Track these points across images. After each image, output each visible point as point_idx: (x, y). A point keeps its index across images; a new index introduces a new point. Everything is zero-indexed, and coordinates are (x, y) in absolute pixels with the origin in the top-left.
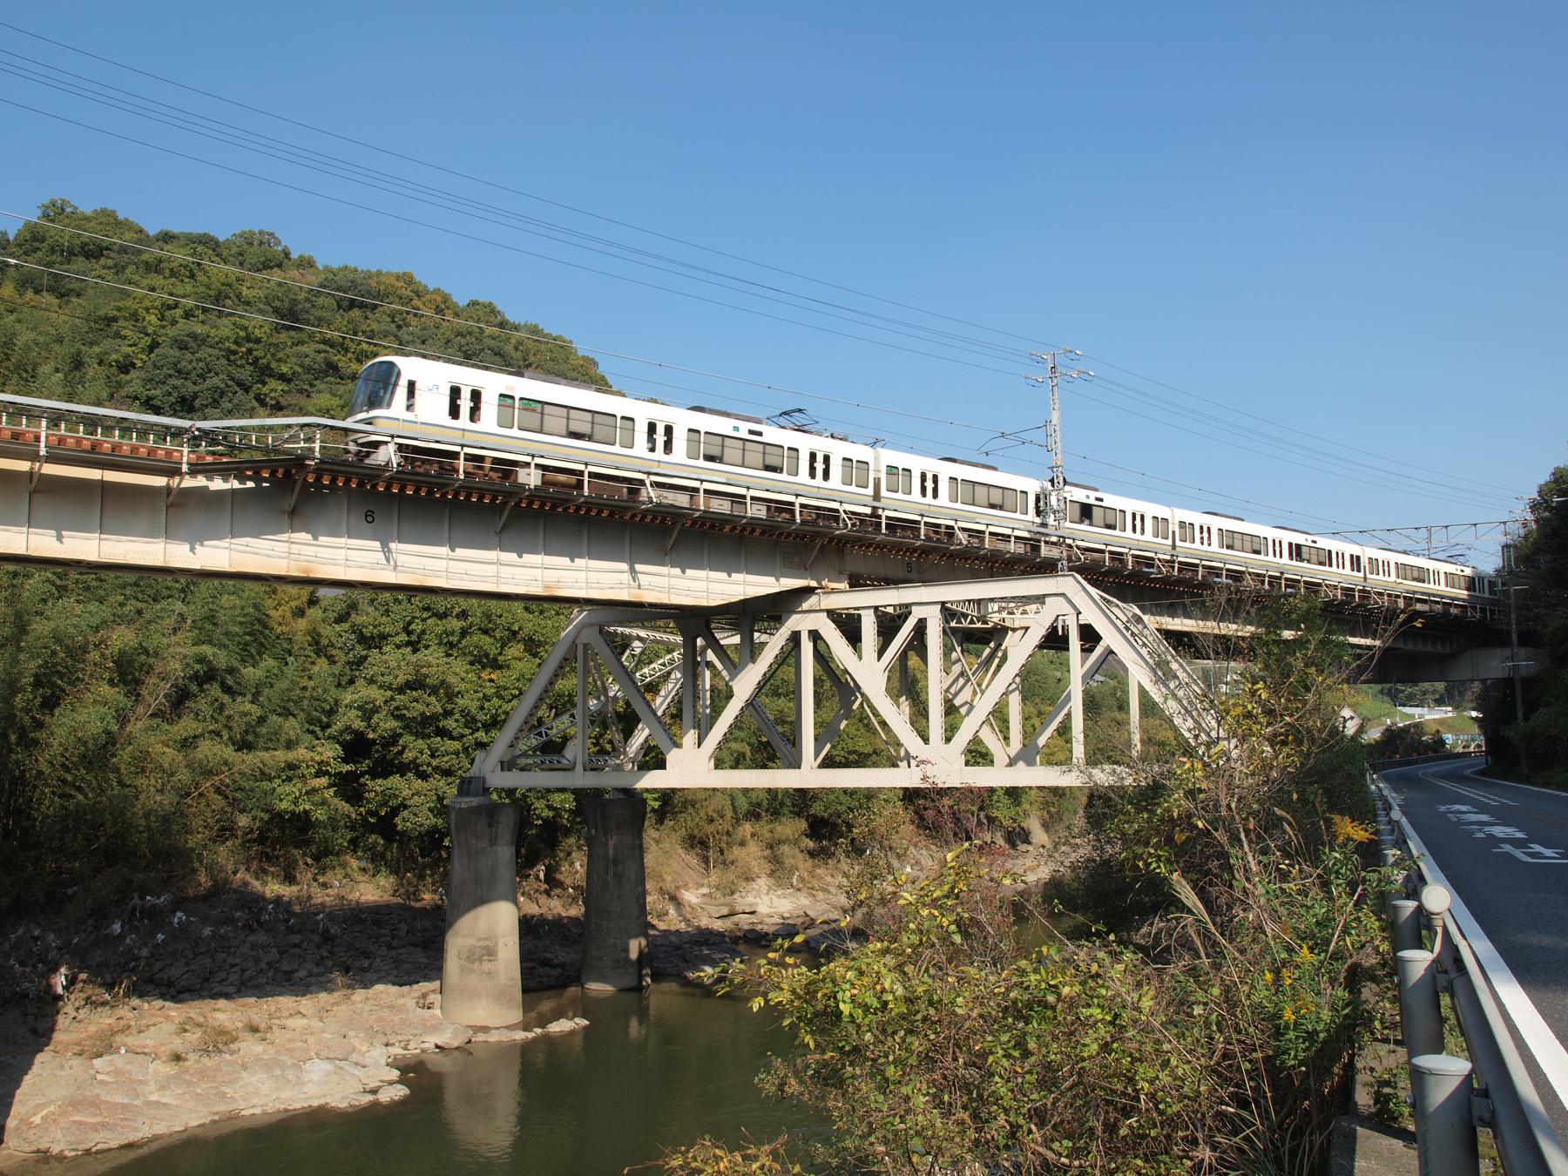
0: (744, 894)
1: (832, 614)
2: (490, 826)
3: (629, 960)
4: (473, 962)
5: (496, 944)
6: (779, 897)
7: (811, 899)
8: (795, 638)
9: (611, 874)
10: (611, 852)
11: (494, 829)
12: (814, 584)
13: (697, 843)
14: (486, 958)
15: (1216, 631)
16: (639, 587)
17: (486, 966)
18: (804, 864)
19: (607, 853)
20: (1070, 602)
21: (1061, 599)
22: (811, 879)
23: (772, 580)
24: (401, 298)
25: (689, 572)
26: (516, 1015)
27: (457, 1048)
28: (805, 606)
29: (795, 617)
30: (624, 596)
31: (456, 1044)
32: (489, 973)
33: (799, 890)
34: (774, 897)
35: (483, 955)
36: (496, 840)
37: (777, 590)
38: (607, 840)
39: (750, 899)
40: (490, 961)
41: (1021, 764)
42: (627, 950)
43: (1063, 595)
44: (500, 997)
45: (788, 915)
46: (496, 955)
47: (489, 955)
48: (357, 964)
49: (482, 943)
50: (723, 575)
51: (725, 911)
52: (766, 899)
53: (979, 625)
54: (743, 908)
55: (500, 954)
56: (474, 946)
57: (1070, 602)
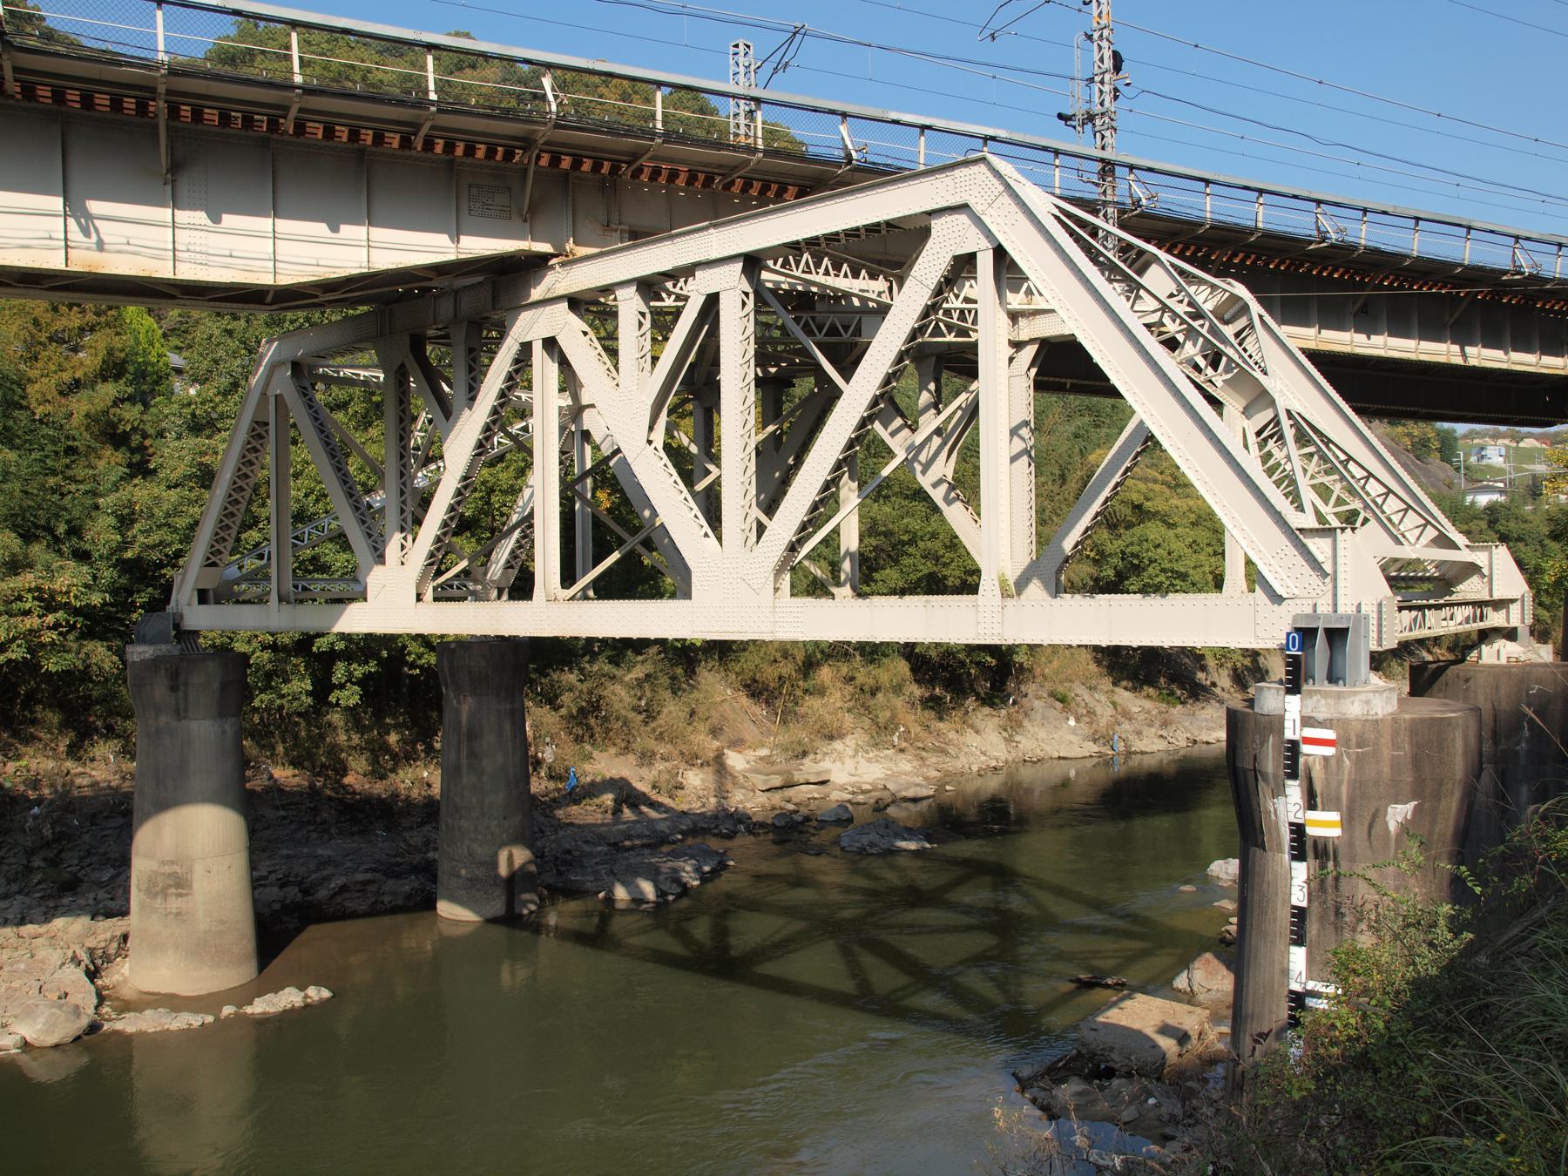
0: (819, 757)
1: (576, 303)
2: (174, 688)
3: (497, 876)
4: (155, 896)
5: (191, 871)
6: (869, 760)
7: (916, 763)
8: (524, 356)
9: (464, 753)
10: (464, 718)
11: (181, 694)
12: (545, 248)
13: (756, 690)
14: (173, 890)
15: (1459, 361)
16: (100, 245)
17: (174, 904)
18: (911, 720)
19: (459, 722)
20: (978, 221)
21: (962, 219)
22: (923, 735)
23: (442, 240)
24: (587, 86)
25: (229, 220)
26: (237, 972)
27: (56, 1046)
28: (536, 294)
29: (525, 316)
30: (54, 261)
31: (51, 1040)
32: (178, 914)
33: (902, 751)
34: (863, 761)
35: (169, 886)
36: (186, 709)
37: (452, 257)
38: (459, 703)
39: (826, 764)
40: (180, 895)
41: (1035, 589)
42: (495, 865)
43: (963, 208)
44: (201, 950)
45: (869, 787)
46: (190, 887)
47: (178, 885)
48: (95, 876)
49: (167, 869)
50: (320, 229)
51: (777, 781)
52: (849, 763)
53: (950, 338)
54: (806, 776)
55: (196, 885)
56: (156, 873)
57: (978, 221)
